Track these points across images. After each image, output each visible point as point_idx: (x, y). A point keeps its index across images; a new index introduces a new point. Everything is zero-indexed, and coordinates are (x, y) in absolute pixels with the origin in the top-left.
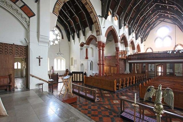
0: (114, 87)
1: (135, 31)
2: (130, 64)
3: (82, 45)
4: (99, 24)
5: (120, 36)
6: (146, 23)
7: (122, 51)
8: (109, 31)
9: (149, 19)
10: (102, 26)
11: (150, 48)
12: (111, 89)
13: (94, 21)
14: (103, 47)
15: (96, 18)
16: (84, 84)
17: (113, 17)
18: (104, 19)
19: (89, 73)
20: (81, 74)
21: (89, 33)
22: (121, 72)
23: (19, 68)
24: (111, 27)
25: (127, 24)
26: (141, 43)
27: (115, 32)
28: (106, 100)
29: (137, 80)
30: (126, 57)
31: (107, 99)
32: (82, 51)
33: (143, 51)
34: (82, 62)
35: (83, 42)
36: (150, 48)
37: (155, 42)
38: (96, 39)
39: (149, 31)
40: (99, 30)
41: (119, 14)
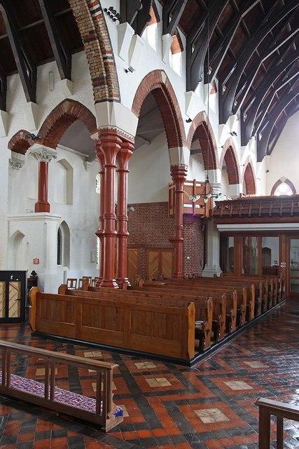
0: (184, 341)
1: (238, 111)
2: (224, 237)
3: (20, 145)
4: (107, 48)
5: (190, 121)
6: (277, 87)
7: (194, 182)
8: (148, 90)
9: (287, 70)
10: (121, 62)
11: (288, 182)
12: (171, 349)
13: (83, 31)
14: (122, 156)
15: (94, 19)
16: (28, 334)
17: (164, 32)
18: (130, 31)
19: (53, 279)
20: (16, 284)
21: (57, 92)
22: (188, 273)
24: (157, 73)
25: (214, 78)
27: (170, 100)
28: (160, 410)
29: (260, 300)
30: (210, 211)
31: (164, 403)
32: (18, 173)
33: (261, 191)
34: (16, 227)
35: (25, 132)
36: (288, 182)
38: (90, 120)
40: (108, 76)
41: (189, 28)
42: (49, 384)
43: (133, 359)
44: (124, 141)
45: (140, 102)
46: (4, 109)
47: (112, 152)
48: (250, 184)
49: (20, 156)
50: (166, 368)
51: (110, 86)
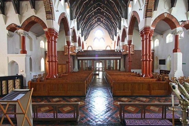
2: (78, 60)
3: (12, 29)
8: (61, 18)
10: (55, 9)
14: (56, 37)
21: (29, 13)
22: (70, 71)
23: (98, 63)
26: (7, 53)
32: (11, 39)
33: (85, 49)
37: (94, 41)
39: (90, 31)
40: (52, 12)
42: (143, 114)
43: (69, 98)
44: (56, 33)
45: (60, 21)
46: (3, 13)
47: (53, 36)
48: (83, 48)
49: (12, 33)
50: (80, 99)
51: (52, 15)
